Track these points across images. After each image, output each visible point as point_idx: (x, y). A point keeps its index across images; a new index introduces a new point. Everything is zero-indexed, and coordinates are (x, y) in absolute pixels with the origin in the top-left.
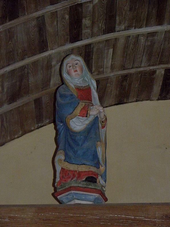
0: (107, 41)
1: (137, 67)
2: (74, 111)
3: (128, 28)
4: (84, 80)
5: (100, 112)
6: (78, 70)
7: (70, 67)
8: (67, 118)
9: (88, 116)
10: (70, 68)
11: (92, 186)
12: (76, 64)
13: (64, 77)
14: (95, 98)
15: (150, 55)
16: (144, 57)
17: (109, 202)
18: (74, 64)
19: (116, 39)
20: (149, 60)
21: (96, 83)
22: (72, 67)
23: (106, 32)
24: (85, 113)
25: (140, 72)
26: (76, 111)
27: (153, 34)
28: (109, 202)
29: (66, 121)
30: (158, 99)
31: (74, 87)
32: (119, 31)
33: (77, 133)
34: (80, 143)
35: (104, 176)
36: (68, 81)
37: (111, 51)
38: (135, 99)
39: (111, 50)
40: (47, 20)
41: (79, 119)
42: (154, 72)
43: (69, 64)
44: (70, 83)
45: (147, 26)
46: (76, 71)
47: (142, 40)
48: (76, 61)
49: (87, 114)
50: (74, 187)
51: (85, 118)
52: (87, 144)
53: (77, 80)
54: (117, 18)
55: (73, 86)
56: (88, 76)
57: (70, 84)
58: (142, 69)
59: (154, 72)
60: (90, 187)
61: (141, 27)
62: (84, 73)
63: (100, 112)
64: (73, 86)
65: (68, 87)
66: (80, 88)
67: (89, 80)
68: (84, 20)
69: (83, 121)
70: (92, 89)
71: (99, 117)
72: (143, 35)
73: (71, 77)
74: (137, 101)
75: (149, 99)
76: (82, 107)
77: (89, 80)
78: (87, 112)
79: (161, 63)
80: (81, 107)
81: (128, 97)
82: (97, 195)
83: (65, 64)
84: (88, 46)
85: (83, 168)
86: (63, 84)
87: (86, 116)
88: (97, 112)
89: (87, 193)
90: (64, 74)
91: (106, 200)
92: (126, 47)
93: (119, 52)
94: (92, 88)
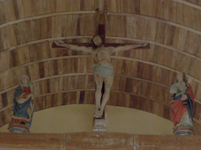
0: (55, 78)
1: (69, 90)
3: (63, 74)
9: (26, 98)
11: (23, 125)
15: (73, 85)
16: (71, 86)
17: (30, 132)
19: (59, 78)
20: (73, 87)
23: (54, 75)
24: (24, 97)
25: (70, 92)
27: (73, 76)
28: (30, 132)
30: (79, 104)
32: (60, 74)
33: (20, 104)
34: (21, 108)
35: (30, 123)
38: (70, 103)
39: (57, 82)
40: (30, 67)
42: (76, 92)
45: (71, 73)
47: (70, 79)
50: (15, 125)
52: (23, 109)
54: (59, 69)
58: (70, 91)
59: (76, 92)
60: (22, 126)
61: (69, 73)
68: (45, 69)
72: (70, 76)
74: (70, 104)
75: (75, 103)
79: (78, 88)
81: (67, 102)
82: (24, 129)
84: (48, 80)
85: (20, 118)
86: (95, 118)
89: (17, 128)
91: (29, 131)
92: (64, 81)
93: (61, 82)
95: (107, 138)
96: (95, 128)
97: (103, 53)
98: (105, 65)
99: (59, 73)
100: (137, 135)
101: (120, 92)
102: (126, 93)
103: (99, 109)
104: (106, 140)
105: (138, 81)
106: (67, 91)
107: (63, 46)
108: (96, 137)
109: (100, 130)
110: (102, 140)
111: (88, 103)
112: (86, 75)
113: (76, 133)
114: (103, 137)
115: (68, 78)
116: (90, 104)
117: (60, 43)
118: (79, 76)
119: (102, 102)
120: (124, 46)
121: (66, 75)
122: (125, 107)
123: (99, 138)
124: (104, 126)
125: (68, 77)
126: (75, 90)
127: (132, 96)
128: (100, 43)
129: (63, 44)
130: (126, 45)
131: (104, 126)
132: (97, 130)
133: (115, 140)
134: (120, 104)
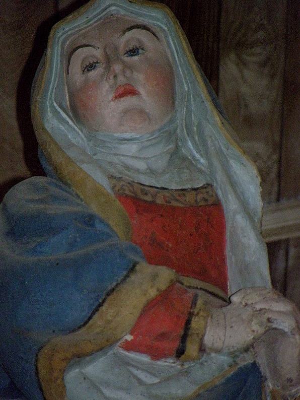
2: (96, 310)
4: (177, 158)
5: (272, 336)
6: (141, 90)
7: (91, 67)
8: (45, 350)
9: (192, 349)
10: (93, 74)
12: (133, 52)
13: (48, 127)
14: (245, 269)
18: (116, 49)
21: (259, 180)
22: (99, 70)
26: (110, 312)
29: (36, 366)
31: (109, 190)
36: (71, 154)
37: (136, 9)
41: (128, 364)
43: (81, 53)
44: (83, 162)
46: (129, 91)
48: (128, 35)
49: (184, 339)
51: (168, 364)
53: (133, 148)
55: (105, 183)
56: (209, 129)
57: (85, 167)
62: (181, 115)
63: (272, 336)
64: (105, 183)
65: (66, 184)
66: (148, 198)
67: (216, 162)
69: (156, 380)
70: (228, 216)
71: (265, 370)
73: (90, 138)
76: (153, 293)
77: (216, 162)
78: (188, 323)
80: (145, 293)
83: (55, 53)
87: (180, 353)
88: (255, 327)
90: (50, 115)
94: (231, 205)
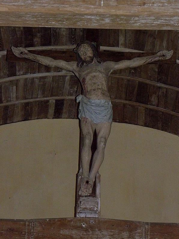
20: (43, 93)
30: (53, 118)
45: (39, 72)
47: (37, 81)
59: (48, 101)
72: (37, 78)
79: (52, 96)
95: (99, 230)
96: (81, 213)
97: (95, 76)
98: (98, 101)
99: (18, 73)
100: (147, 223)
101: (127, 102)
102: (138, 104)
103: (87, 182)
104: (98, 232)
105: (160, 88)
106: (31, 100)
107: (26, 56)
108: (82, 227)
109: (89, 216)
110: (91, 232)
111: (69, 117)
112: (66, 76)
113: (50, 220)
114: (92, 228)
115: (34, 80)
116: (74, 118)
117: (22, 53)
118: (54, 77)
119: (91, 169)
120: (132, 60)
121: (30, 76)
122: (137, 125)
123: (86, 230)
124: (96, 209)
125: (33, 78)
126: (45, 99)
127: (147, 110)
128: (90, 57)
129: (26, 54)
130: (136, 59)
131: (96, 209)
132: (83, 215)
133: (112, 234)
134: (127, 121)
